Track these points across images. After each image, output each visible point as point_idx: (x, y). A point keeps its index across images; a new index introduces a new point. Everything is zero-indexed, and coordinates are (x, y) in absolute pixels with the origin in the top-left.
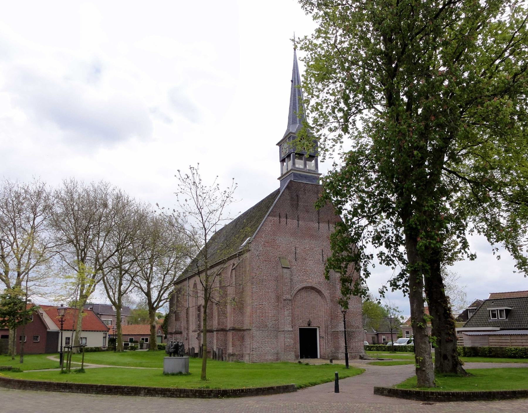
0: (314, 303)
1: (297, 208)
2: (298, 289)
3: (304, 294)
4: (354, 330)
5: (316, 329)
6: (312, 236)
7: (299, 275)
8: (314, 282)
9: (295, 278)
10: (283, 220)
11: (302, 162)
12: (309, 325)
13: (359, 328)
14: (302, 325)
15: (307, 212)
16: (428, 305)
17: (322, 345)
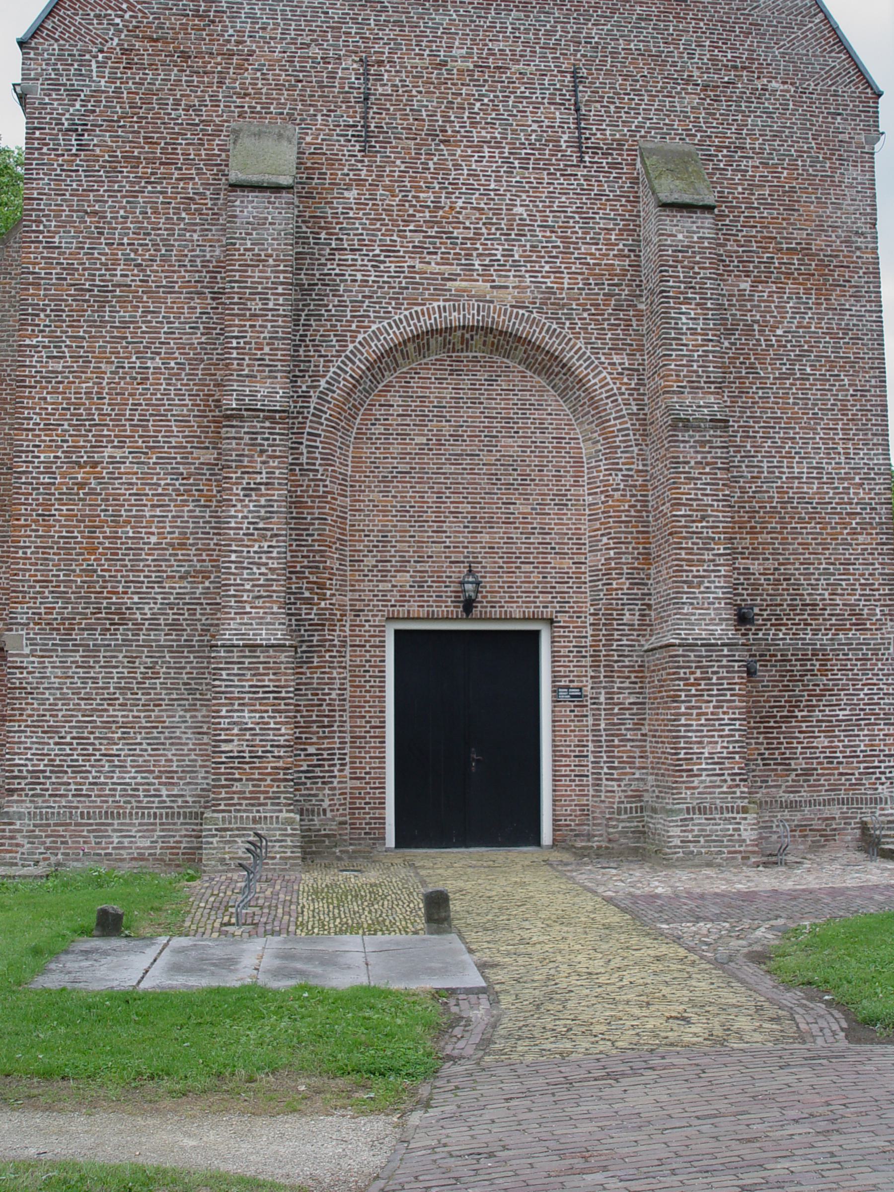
0: (511, 445)
4: (824, 639)
5: (536, 634)
7: (389, 251)
8: (510, 297)
9: (354, 275)
12: (468, 605)
13: (860, 625)
14: (414, 608)
16: (363, 998)
17: (567, 750)
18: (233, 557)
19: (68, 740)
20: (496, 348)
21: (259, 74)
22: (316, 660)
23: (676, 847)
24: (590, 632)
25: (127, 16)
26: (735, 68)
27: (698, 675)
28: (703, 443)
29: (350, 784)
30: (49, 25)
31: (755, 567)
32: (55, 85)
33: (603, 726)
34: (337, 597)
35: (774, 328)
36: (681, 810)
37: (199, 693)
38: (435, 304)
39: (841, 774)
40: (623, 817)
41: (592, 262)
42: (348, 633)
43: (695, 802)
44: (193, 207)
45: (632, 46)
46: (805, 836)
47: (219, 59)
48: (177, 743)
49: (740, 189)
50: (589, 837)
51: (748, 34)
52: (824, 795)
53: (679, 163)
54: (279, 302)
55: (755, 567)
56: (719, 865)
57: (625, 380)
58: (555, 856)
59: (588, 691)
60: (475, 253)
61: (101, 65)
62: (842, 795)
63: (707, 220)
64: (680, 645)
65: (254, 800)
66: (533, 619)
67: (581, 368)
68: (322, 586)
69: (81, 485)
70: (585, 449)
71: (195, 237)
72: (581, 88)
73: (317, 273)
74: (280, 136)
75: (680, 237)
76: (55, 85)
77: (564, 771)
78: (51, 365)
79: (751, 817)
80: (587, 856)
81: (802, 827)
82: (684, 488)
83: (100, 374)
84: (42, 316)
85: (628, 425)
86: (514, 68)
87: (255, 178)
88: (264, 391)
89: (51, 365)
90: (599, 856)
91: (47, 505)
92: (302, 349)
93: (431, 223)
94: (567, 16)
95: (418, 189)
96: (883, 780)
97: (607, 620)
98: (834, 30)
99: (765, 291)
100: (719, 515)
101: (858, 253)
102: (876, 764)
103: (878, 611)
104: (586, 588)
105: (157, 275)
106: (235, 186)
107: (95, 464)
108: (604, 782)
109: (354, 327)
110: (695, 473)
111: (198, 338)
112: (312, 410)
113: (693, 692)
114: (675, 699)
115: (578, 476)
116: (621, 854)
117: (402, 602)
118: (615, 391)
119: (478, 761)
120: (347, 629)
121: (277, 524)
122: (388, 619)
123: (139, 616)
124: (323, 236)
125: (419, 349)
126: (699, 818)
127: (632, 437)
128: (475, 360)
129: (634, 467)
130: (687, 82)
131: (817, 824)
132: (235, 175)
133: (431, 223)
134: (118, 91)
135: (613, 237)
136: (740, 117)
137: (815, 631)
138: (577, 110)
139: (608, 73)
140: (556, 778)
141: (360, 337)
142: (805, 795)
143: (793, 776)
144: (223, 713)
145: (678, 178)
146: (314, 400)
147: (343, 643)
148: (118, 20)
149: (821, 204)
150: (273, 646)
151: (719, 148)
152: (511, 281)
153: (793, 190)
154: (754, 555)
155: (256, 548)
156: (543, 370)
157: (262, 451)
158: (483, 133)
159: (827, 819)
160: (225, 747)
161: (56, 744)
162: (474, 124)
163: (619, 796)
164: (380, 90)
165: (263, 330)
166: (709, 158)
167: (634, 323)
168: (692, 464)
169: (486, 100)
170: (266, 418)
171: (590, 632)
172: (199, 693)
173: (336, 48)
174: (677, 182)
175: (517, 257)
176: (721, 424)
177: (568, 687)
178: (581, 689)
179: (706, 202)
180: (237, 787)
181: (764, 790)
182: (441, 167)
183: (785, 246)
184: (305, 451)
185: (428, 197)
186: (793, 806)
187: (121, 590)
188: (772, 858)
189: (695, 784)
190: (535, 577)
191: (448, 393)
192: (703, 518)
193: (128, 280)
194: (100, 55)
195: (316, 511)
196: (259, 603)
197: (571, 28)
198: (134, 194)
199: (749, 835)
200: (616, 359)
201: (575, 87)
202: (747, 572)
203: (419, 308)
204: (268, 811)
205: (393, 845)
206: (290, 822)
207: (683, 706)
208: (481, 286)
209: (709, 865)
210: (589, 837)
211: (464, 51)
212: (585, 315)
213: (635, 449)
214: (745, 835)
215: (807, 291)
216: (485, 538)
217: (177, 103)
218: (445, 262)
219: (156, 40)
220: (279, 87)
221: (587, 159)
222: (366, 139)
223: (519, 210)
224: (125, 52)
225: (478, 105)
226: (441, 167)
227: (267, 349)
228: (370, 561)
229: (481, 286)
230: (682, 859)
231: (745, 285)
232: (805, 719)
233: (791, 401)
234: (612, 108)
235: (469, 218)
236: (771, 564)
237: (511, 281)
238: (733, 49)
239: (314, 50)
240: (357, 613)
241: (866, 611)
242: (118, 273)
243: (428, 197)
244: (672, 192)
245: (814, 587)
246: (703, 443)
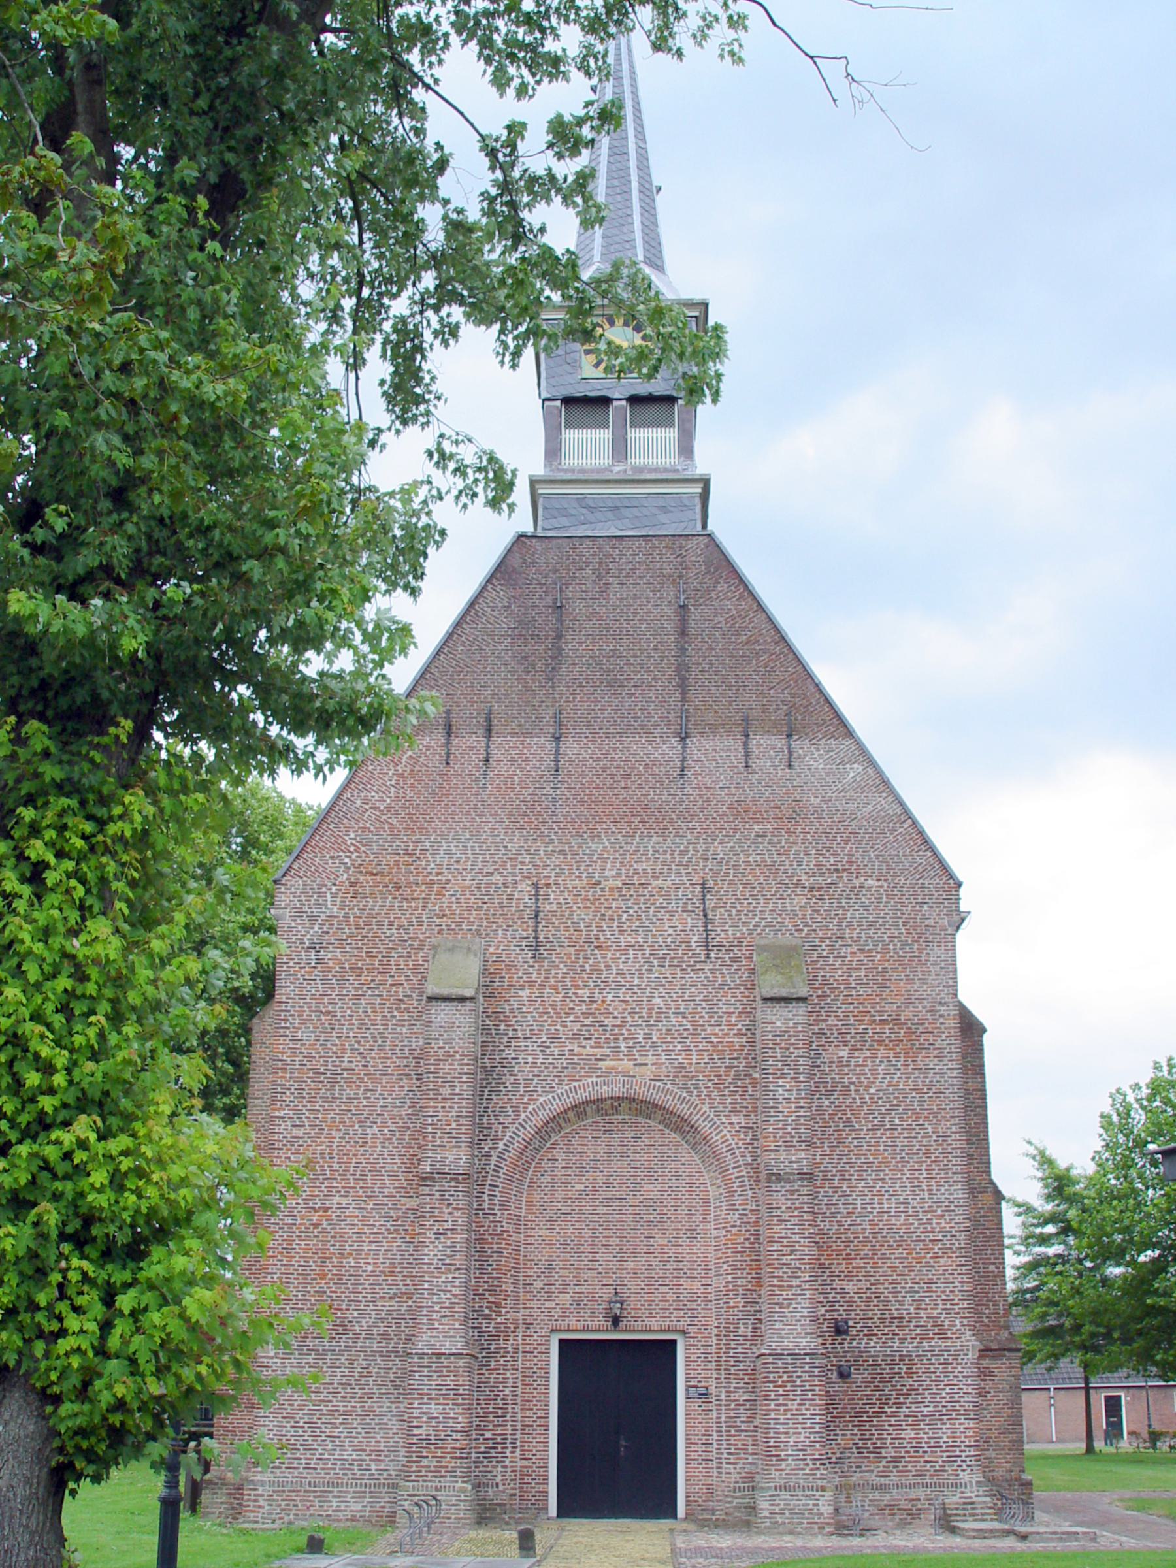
0: (651, 1190)
1: (551, 675)
2: (543, 1115)
3: (590, 1143)
5: (674, 1342)
6: (647, 817)
7: (554, 1038)
8: (649, 1071)
10: (469, 743)
11: (603, 436)
12: (616, 1321)
14: (573, 1324)
15: (613, 684)
18: (426, 1286)
19: (301, 1424)
20: (639, 1112)
21: (453, 899)
22: (493, 1363)
23: (766, 1517)
24: (715, 1342)
25: (354, 857)
26: (837, 870)
27: (785, 1378)
28: (792, 1192)
29: (520, 1463)
30: (295, 866)
31: (850, 1287)
32: (300, 912)
33: (723, 1419)
34: (509, 1314)
35: (868, 1087)
36: (769, 1488)
37: (401, 1388)
38: (590, 1080)
40: (738, 1494)
41: (715, 1040)
42: (520, 1342)
43: (783, 1482)
44: (403, 1006)
45: (751, 859)
46: (894, 1514)
47: (423, 887)
48: (384, 1427)
49: (840, 972)
50: (713, 1511)
51: (847, 842)
52: (912, 1480)
53: (783, 957)
54: (463, 1088)
55: (850, 1287)
56: (800, 1533)
57: (742, 1136)
58: (685, 1525)
59: (713, 1390)
60: (621, 1038)
61: (334, 896)
62: (928, 1480)
63: (802, 1009)
64: (770, 1355)
65: (437, 1473)
67: (705, 1127)
68: (498, 1305)
69: (316, 1226)
70: (712, 1192)
71: (404, 1030)
72: (708, 897)
73: (497, 1058)
74: (469, 949)
75: (778, 1024)
77: (693, 1455)
78: (295, 1132)
79: (828, 1494)
80: (708, 1526)
81: (891, 1507)
82: (777, 1229)
83: (331, 1138)
84: (288, 1093)
85: (744, 1173)
86: (655, 883)
87: (445, 992)
88: (451, 1158)
89: (295, 1132)
90: (717, 1526)
91: (290, 1241)
92: (485, 1118)
93: (586, 1014)
94: (697, 838)
95: (577, 987)
96: (964, 1467)
97: (727, 1332)
98: (921, 833)
99: (860, 1057)
100: (806, 1249)
101: (942, 1020)
102: (958, 1453)
103: (958, 1322)
104: (711, 1305)
105: (375, 1061)
106: (430, 999)
107: (326, 1210)
108: (724, 1465)
109: (525, 1100)
110: (786, 1216)
111: (406, 1111)
112: (492, 1167)
113: (781, 1392)
114: (766, 1398)
115: (706, 1214)
116: (735, 1525)
117: (564, 1317)
118: (734, 1146)
119: (626, 1447)
120: (520, 1338)
121: (459, 1260)
122: (552, 1330)
123: (357, 1328)
124: (502, 1027)
125: (578, 1115)
126: (785, 1495)
127: (747, 1183)
128: (624, 1121)
129: (748, 1207)
130: (797, 885)
131: (904, 1504)
132: (431, 989)
133: (586, 1014)
134: (346, 916)
135: (733, 1019)
136: (840, 912)
137: (902, 1341)
138: (705, 915)
139: (731, 883)
140: (688, 1461)
141: (530, 1108)
142: (894, 1479)
143: (884, 1463)
144: (416, 1405)
145: (781, 973)
146: (494, 1158)
148: (347, 860)
149: (909, 981)
150: (454, 1354)
151: (822, 940)
152: (650, 1060)
153: (885, 970)
154: (849, 1277)
155: (443, 1279)
156: (677, 1129)
157: (449, 1205)
158: (629, 939)
159: (913, 1500)
161: (293, 1427)
162: (622, 932)
163: (735, 1477)
164: (548, 908)
165: (452, 1111)
166: (814, 948)
167: (750, 1089)
168: (784, 1208)
169: (631, 911)
170: (452, 1179)
171: (715, 1342)
172: (401, 1388)
173: (514, 874)
174: (779, 977)
175: (655, 1040)
176: (808, 1176)
177: (696, 1387)
178: (707, 1388)
179: (799, 995)
180: (425, 1462)
181: (858, 1474)
182: (595, 969)
183: (878, 1018)
184: (487, 1199)
185: (585, 993)
186: (882, 1488)
187: (344, 1307)
188: (842, 1528)
189: (783, 1467)
190: (671, 1297)
191: (602, 1149)
192: (792, 1252)
193: (353, 1066)
194: (334, 888)
195: (495, 1246)
196: (445, 1320)
197: (701, 847)
198: (357, 997)
199: (826, 1509)
200: (734, 1119)
201: (704, 896)
202: (843, 1292)
203: (576, 1084)
204: (447, 1481)
205: (555, 1514)
206: (464, 1490)
207: (772, 1403)
208: (627, 1064)
209: (791, 1533)
210: (713, 1511)
211: (614, 873)
212: (710, 1084)
213: (750, 1193)
214: (822, 1509)
215: (897, 1055)
216: (631, 1265)
217: (391, 924)
218: (598, 1045)
219: (375, 875)
220: (469, 909)
221: (713, 955)
222: (536, 947)
223: (657, 1000)
224: (352, 884)
225: (625, 916)
226: (595, 969)
227: (454, 1125)
228: (539, 1284)
229: (627, 1064)
230: (769, 1528)
231: (844, 1053)
233: (882, 1148)
234: (734, 912)
235: (617, 1009)
236: (864, 1285)
237: (650, 1060)
238: (835, 855)
239: (497, 878)
240: (528, 1325)
241: (947, 1323)
242: (346, 1059)
243: (585, 993)
244: (772, 987)
245: (901, 1303)
246: (792, 1192)
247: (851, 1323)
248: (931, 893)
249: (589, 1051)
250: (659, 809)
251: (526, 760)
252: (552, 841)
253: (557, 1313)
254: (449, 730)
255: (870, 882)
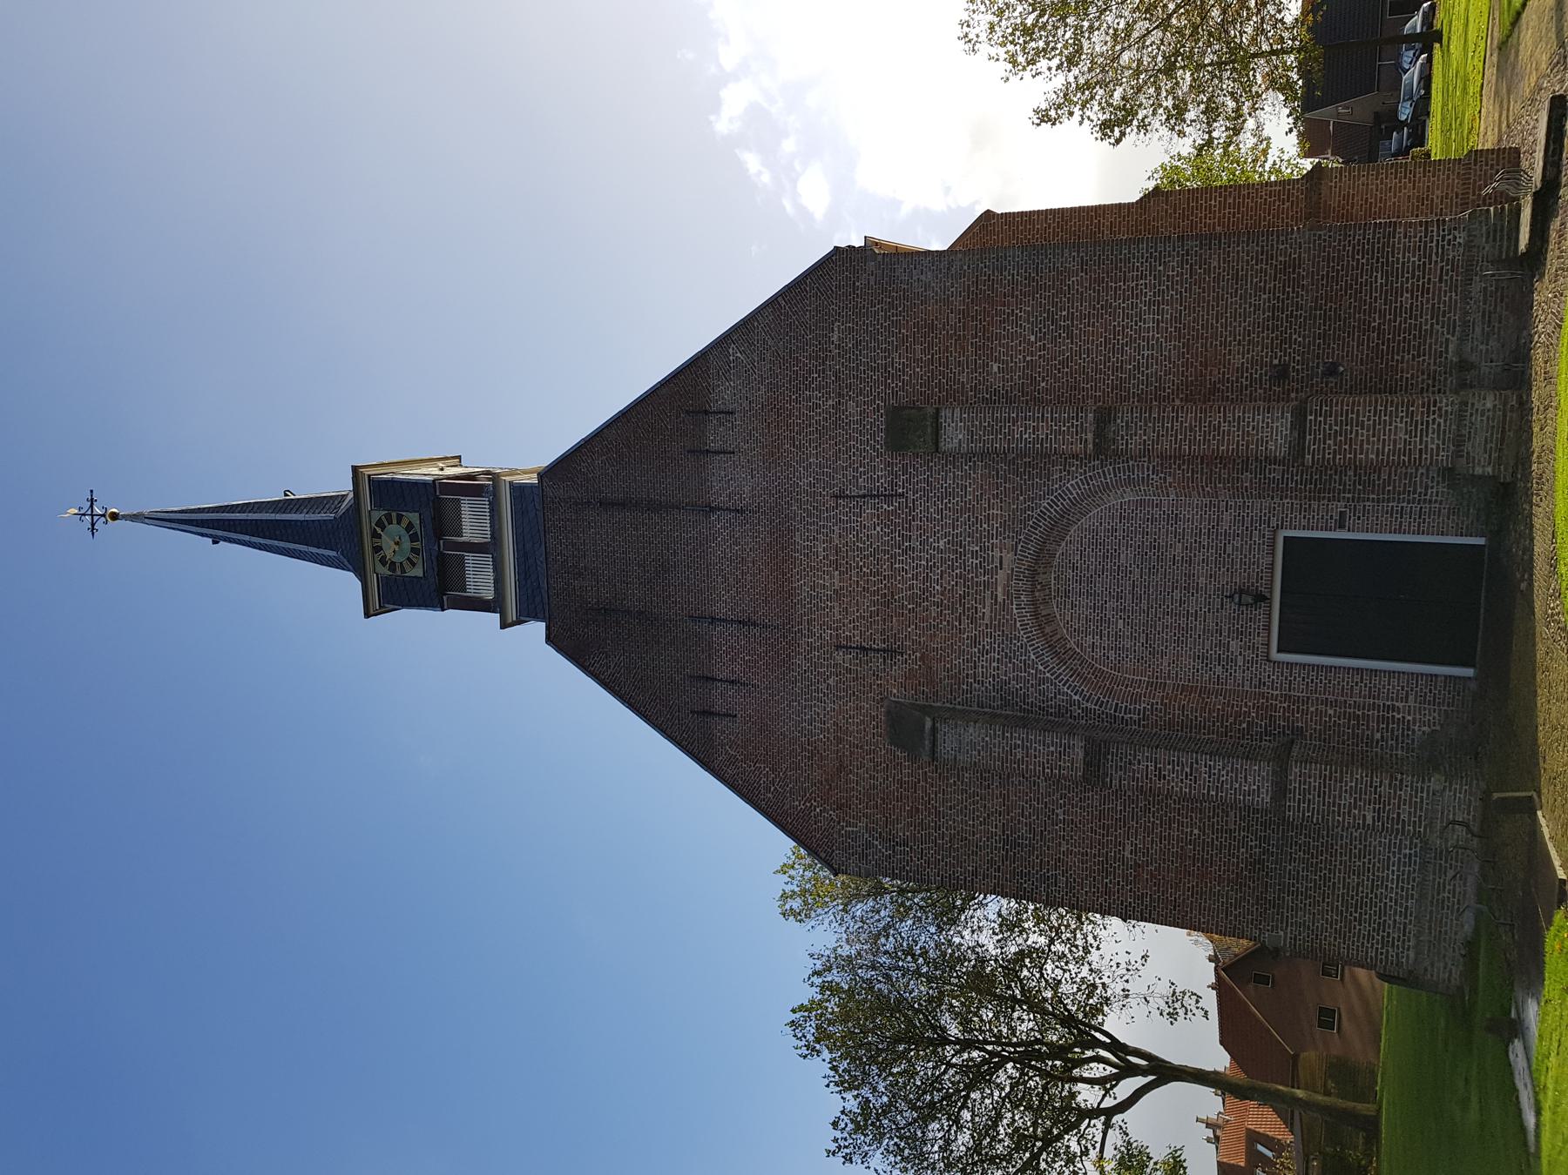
7: (975, 642)
8: (1008, 557)
35: (1030, 344)
39: (1441, 281)
66: (1273, 545)
68: (1238, 714)
76: (863, 856)
117: (1254, 648)
147: (1287, 698)
151: (887, 386)
160: (1369, 821)
182: (911, 599)
185: (934, 611)
198: (937, 814)
208: (1001, 576)
216: (1202, 580)
222: (891, 652)
226: (911, 599)
229: (1001, 576)
232: (1382, 315)
238: (810, 372)
240: (1261, 683)
243: (934, 611)
247: (1276, 362)
248: (855, 281)
249: (987, 610)
250: (772, 534)
251: (731, 647)
252: (800, 631)
253: (1249, 655)
254: (708, 713)
255: (835, 338)
